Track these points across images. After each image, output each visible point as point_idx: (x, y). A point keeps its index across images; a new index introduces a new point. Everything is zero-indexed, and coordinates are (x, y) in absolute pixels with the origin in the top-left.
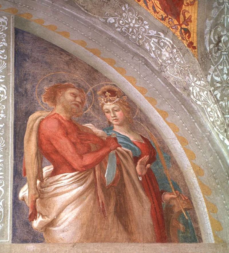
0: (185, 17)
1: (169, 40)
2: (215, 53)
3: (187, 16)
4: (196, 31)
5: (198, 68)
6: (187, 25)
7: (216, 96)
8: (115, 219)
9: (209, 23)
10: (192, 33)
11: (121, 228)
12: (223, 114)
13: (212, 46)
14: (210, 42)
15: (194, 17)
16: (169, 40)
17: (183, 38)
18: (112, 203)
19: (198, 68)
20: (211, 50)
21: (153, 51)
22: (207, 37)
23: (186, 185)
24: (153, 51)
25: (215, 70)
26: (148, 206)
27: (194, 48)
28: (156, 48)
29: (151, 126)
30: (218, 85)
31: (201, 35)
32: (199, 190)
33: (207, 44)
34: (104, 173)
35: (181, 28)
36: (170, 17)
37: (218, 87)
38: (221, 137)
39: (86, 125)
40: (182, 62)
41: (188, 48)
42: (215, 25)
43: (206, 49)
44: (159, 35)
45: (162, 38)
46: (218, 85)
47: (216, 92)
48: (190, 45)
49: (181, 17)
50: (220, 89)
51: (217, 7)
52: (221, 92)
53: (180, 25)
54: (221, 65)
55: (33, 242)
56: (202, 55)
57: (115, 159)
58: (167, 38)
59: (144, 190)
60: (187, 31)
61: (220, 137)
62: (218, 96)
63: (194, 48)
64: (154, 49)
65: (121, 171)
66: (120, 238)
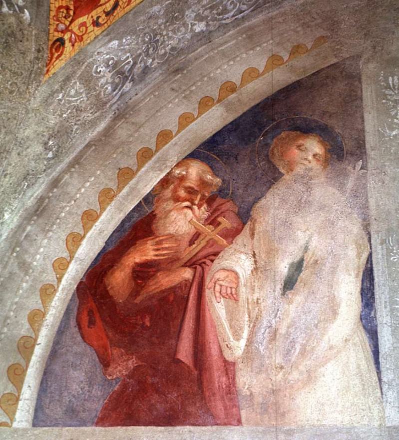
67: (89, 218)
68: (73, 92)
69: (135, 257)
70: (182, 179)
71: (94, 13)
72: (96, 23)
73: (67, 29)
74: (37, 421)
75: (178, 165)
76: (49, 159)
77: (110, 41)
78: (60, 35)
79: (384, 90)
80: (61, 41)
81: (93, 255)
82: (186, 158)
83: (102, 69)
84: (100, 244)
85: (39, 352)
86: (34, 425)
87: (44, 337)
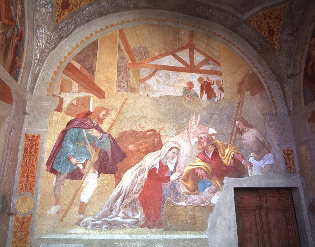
0: (64, 12)
1: (51, 10)
2: (59, 30)
3: (65, 13)
4: (62, 19)
5: (52, 28)
6: (62, 15)
7: (48, 41)
8: (3, 54)
9: (66, 21)
10: (61, 18)
11: (3, 59)
12: (45, 48)
13: (60, 27)
14: (61, 26)
15: (66, 15)
16: (51, 10)
17: (57, 16)
18: (6, 46)
19: (52, 28)
20: (59, 28)
21: (40, 3)
22: (62, 24)
23: (22, 59)
24: (40, 3)
25: (54, 34)
26: (12, 57)
27: (57, 22)
28: (42, 4)
29: (25, 28)
30: (51, 39)
31: (62, 22)
32: (24, 63)
33: (60, 25)
34: (159, 172)
35: (60, 14)
36: (61, 7)
37: (51, 39)
38: (37, 52)
39: (11, 6)
40: (48, 20)
41: (55, 20)
42: (67, 24)
43: (59, 26)
44: (49, 4)
45: (49, 6)
46: (51, 39)
47: (49, 40)
48: (57, 21)
49: (64, 11)
50: (50, 40)
51: (71, 20)
52: (50, 41)
53: (61, 13)
54: (57, 34)
55: (192, 239)
56: (56, 27)
57: (12, 30)
58: (50, 8)
59: (14, 50)
60: (60, 16)
61: (37, 51)
62: (48, 42)
63: (57, 22)
64: (41, 3)
65: (12, 36)
66: (2, 62)
67: (301, 62)
68: (284, 46)
69: (310, 65)
70: (312, 44)
71: (276, 34)
72: (277, 34)
73: (273, 41)
74: (305, 105)
75: (310, 41)
76: (290, 58)
77: (283, 33)
78: (272, 43)
79: (10, 177)
80: (274, 43)
81: (304, 69)
82: (311, 39)
83: (286, 38)
84: (109, 238)
85: (302, 92)
86: (305, 106)
87: (302, 90)
